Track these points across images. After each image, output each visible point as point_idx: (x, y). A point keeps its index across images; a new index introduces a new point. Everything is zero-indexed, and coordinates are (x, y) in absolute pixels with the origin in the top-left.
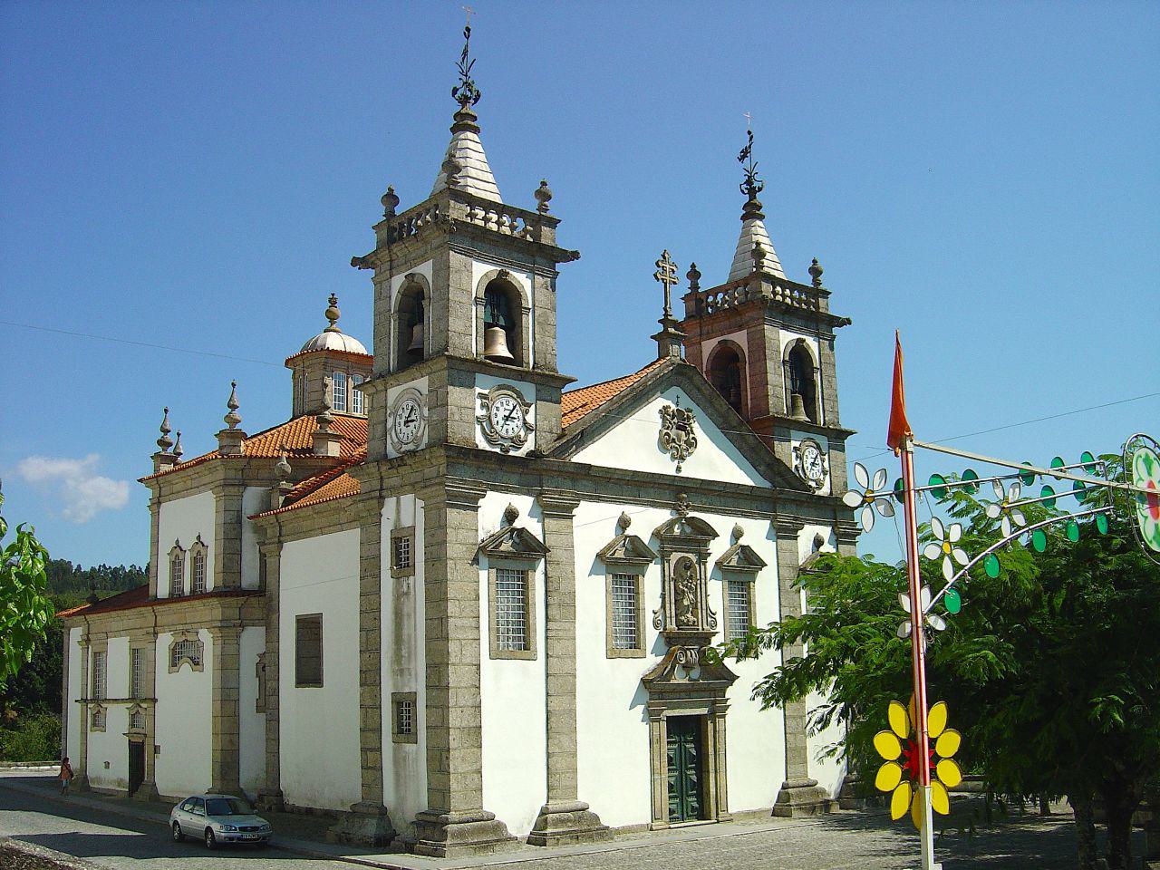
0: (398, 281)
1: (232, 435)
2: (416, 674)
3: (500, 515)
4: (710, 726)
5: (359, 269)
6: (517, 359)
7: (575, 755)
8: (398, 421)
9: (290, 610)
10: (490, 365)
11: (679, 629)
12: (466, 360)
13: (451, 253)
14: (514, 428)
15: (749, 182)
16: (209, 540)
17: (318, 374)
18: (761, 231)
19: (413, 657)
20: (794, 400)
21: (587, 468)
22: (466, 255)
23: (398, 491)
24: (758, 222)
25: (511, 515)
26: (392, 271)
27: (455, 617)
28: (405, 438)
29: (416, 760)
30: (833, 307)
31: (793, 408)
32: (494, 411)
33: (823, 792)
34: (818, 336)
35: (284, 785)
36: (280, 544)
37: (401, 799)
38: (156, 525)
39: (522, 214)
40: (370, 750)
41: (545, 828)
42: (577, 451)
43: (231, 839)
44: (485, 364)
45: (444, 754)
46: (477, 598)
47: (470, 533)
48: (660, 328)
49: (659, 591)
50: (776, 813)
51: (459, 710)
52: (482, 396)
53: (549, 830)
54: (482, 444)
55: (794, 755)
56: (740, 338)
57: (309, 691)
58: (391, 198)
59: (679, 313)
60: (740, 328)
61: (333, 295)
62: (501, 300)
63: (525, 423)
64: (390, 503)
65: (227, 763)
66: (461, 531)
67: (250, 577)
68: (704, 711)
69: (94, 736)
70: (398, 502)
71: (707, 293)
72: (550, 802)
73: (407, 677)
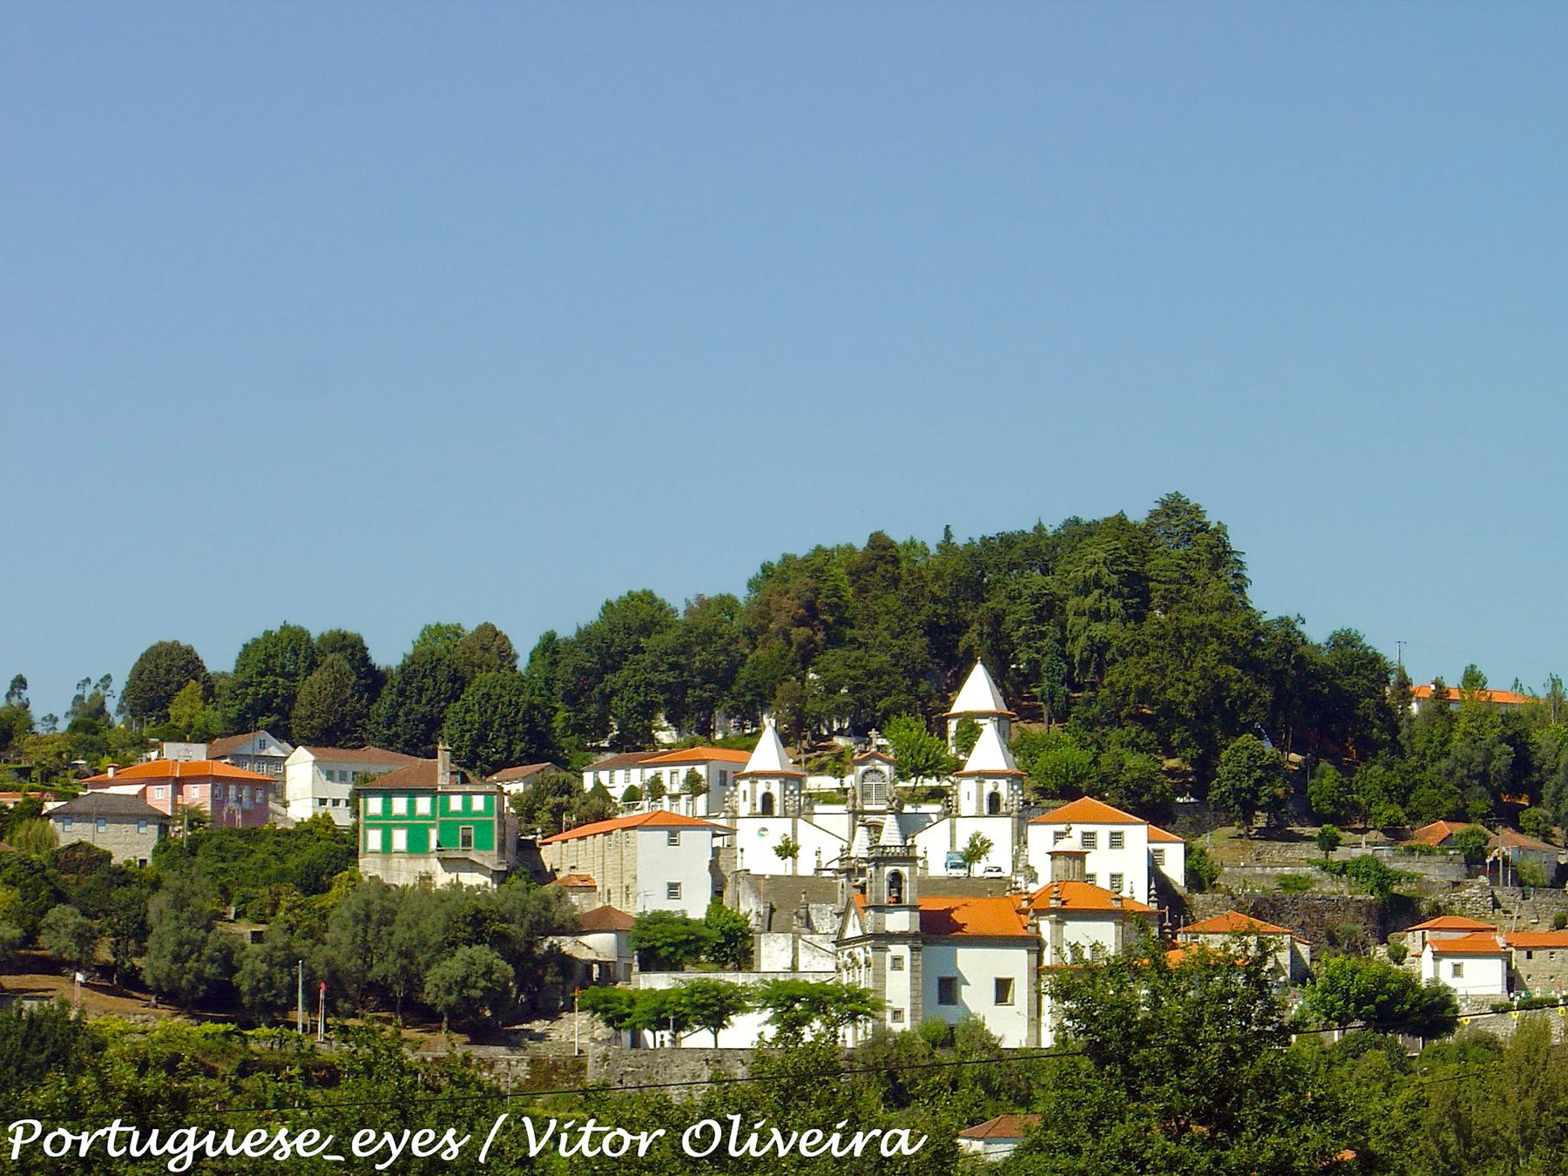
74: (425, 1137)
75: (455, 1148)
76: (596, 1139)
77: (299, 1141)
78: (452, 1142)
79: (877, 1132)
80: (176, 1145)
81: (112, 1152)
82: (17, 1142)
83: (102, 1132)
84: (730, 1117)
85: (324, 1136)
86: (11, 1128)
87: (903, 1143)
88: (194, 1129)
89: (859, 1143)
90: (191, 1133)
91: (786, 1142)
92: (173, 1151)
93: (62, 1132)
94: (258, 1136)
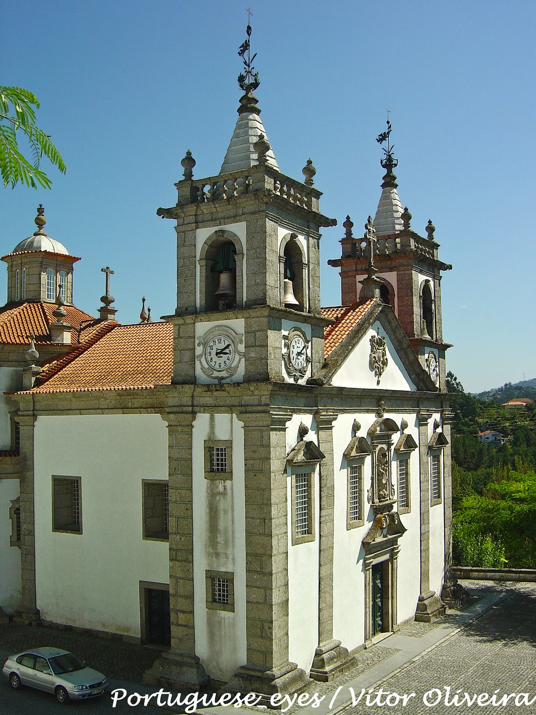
2: (233, 559)
4: (390, 565)
5: (163, 217)
6: (300, 307)
8: (209, 350)
11: (380, 502)
13: (267, 219)
17: (36, 270)
18: (397, 197)
19: (230, 544)
22: (275, 222)
24: (395, 190)
26: (198, 223)
28: (217, 366)
29: (233, 624)
30: (441, 256)
32: (292, 349)
35: (40, 604)
36: (35, 417)
41: (323, 666)
43: (84, 696)
44: (285, 311)
45: (266, 626)
50: (417, 619)
52: (285, 338)
53: (327, 669)
60: (391, 270)
61: (41, 205)
68: (387, 557)
70: (212, 419)
72: (321, 645)
73: (222, 560)
74: (227, 697)
75: (318, 702)
76: (384, 698)
77: (246, 699)
78: (316, 699)
79: (513, 695)
80: (189, 701)
81: (159, 704)
82: (115, 699)
83: (154, 695)
84: (445, 687)
85: (257, 696)
86: (112, 693)
87: (526, 699)
88: (197, 694)
89: (505, 700)
90: (196, 695)
91: (292, 699)
92: (187, 703)
93: (136, 694)
94: (227, 697)
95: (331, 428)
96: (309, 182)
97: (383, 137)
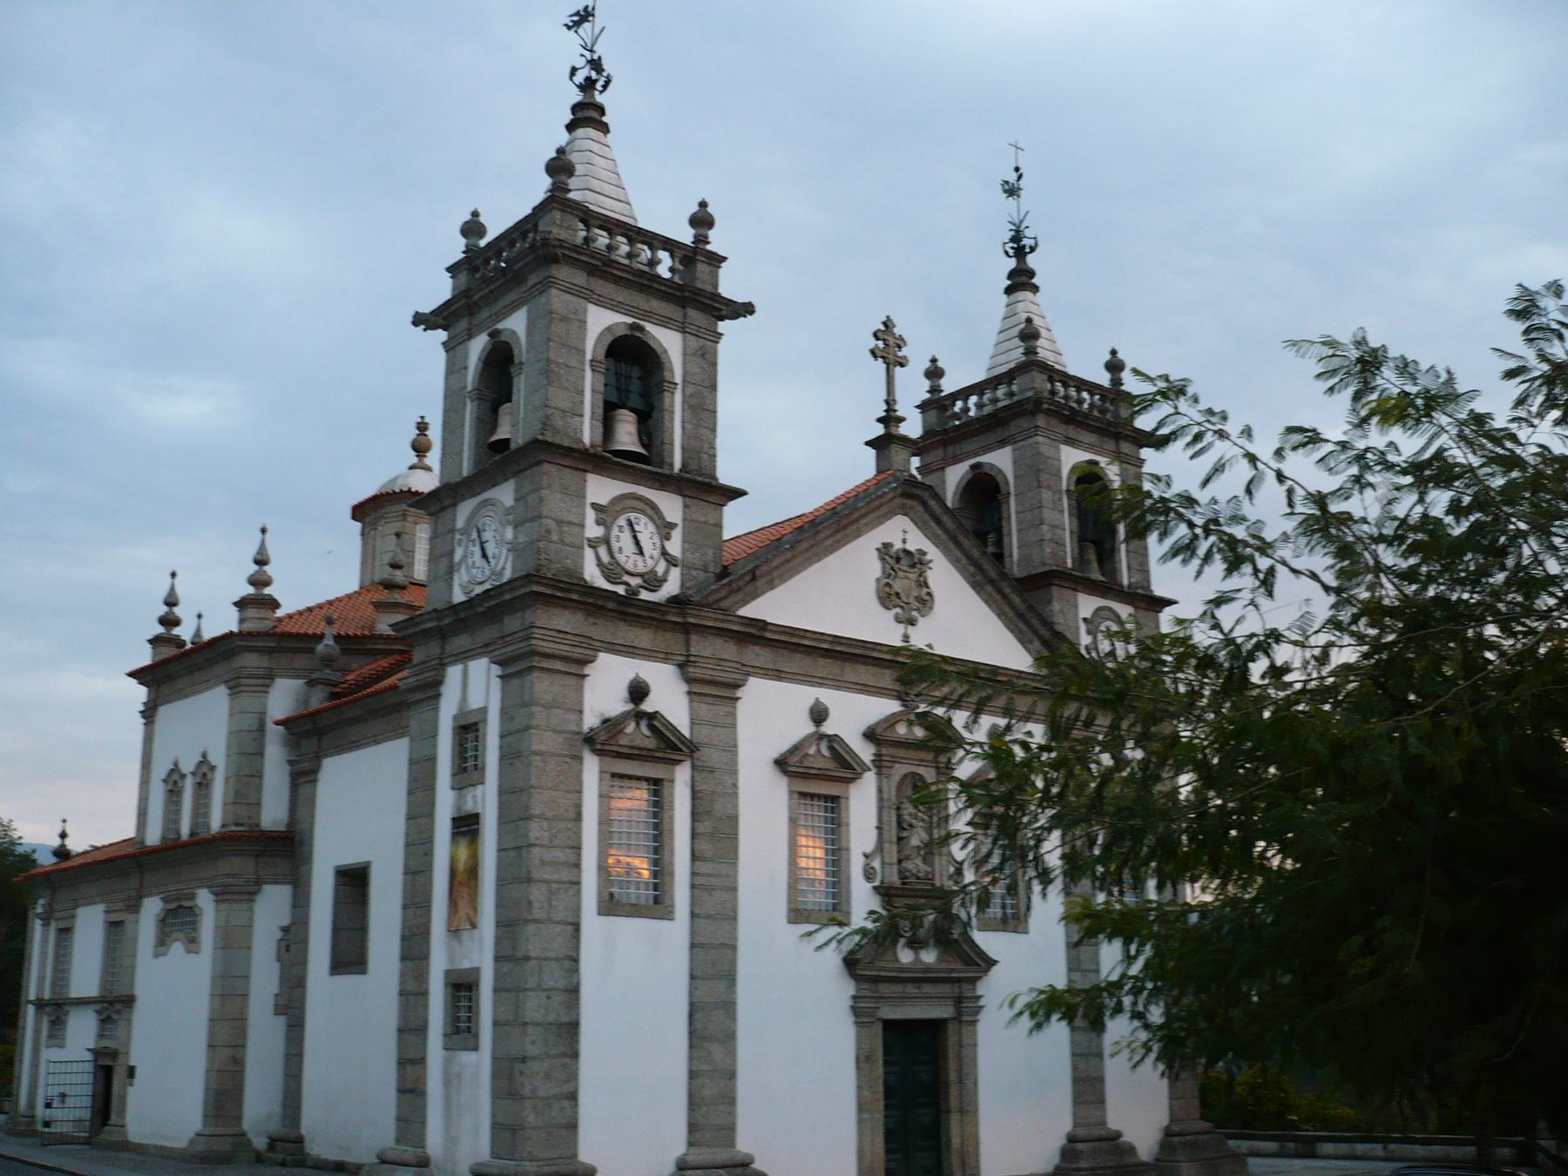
0: (478, 346)
1: (257, 601)
3: (622, 691)
7: (732, 1075)
9: (328, 855)
10: (605, 460)
12: (571, 450)
14: (651, 560)
15: (1017, 238)
16: (218, 758)
20: (1082, 551)
21: (763, 625)
23: (465, 656)
25: (638, 692)
27: (542, 846)
30: (730, 285)
31: (1081, 560)
33: (1131, 1150)
34: (1118, 456)
37: (451, 1141)
38: (148, 740)
39: (669, 245)
40: (410, 1063)
42: (745, 602)
46: (578, 817)
47: (572, 716)
48: (880, 430)
49: (874, 822)
51: (543, 995)
54: (592, 574)
55: (1088, 1087)
56: (1001, 460)
57: (347, 981)
58: (472, 228)
59: (912, 427)
60: (1002, 443)
62: (630, 359)
63: (664, 553)
64: (454, 673)
65: (224, 1094)
66: (556, 711)
67: (273, 813)
69: (48, 1054)
71: (955, 396)
95: (584, 676)
96: (701, 240)
97: (584, 16)
